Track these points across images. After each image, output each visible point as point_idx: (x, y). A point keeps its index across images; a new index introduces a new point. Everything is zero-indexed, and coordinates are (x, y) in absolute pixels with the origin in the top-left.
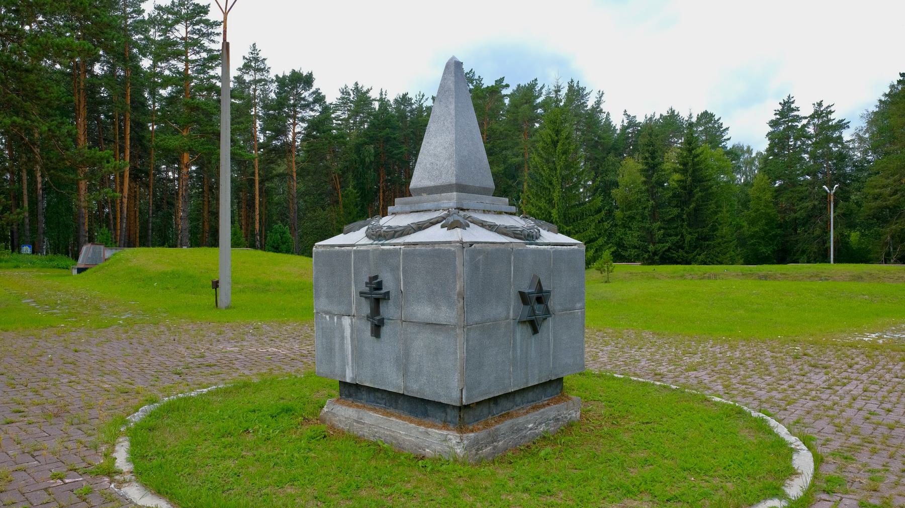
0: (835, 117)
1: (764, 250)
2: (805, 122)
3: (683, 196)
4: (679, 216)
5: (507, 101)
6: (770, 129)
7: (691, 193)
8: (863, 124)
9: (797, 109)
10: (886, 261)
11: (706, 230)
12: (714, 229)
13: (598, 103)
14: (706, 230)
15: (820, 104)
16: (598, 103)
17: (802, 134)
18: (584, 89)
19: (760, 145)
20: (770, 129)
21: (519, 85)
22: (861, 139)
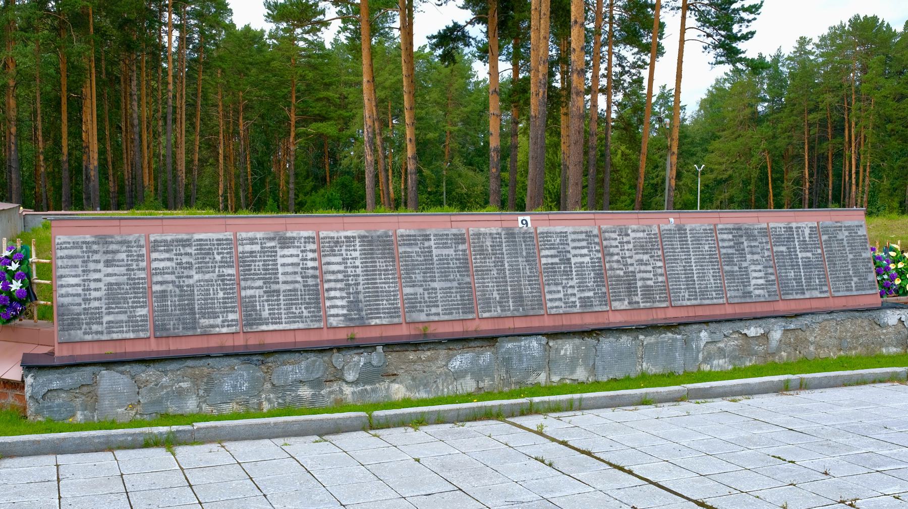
15: (664, 87)
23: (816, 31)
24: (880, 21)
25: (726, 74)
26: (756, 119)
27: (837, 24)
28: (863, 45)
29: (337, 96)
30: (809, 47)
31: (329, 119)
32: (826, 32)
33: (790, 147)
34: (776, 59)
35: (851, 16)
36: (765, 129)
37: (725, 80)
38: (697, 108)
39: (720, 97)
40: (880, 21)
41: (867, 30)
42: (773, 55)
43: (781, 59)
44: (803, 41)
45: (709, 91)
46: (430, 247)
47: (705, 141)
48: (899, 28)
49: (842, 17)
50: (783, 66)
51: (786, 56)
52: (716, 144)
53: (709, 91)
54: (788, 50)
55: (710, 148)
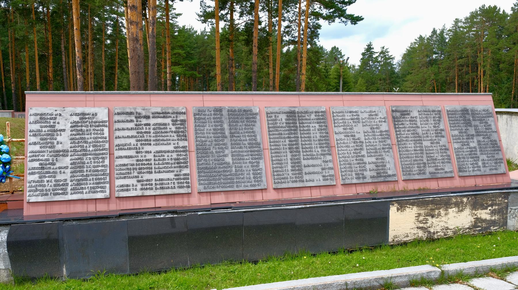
2: (377, 55)
15: (383, 48)
23: (464, 14)
24: (498, 8)
25: (416, 40)
26: (432, 63)
27: (474, 10)
28: (489, 22)
29: (184, 52)
30: (460, 24)
31: (179, 64)
32: (468, 15)
33: (448, 78)
34: (442, 32)
35: (480, 5)
36: (434, 68)
37: (415, 43)
38: (401, 59)
39: (413, 52)
40: (498, 8)
41: (489, 14)
42: (441, 29)
43: (445, 31)
44: (457, 21)
45: (407, 49)
46: (469, 120)
47: (404, 75)
48: (509, 12)
49: (475, 7)
50: (447, 34)
51: (448, 29)
52: (409, 77)
53: (407, 49)
54: (449, 25)
55: (406, 79)
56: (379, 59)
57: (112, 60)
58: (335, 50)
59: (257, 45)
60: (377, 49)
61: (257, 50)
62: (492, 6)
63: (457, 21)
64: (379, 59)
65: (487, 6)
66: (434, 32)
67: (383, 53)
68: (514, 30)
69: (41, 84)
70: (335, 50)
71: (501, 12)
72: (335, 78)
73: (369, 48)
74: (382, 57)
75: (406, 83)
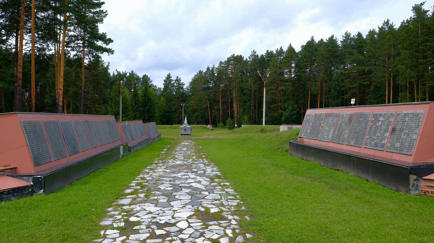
0: (182, 81)
1: (164, 120)
2: (174, 82)
3: (145, 104)
4: (144, 111)
5: (142, 80)
6: (164, 83)
7: (147, 104)
8: (188, 85)
9: (171, 77)
10: (194, 124)
11: (151, 115)
12: (153, 114)
13: (108, 66)
14: (151, 115)
15: (178, 77)
16: (108, 66)
17: (173, 85)
18: (103, 61)
19: (162, 87)
20: (164, 83)
21: (267, 51)
22: (188, 89)
56: (175, 84)
57: (364, 92)
58: (145, 77)
59: (21, 65)
60: (174, 78)
61: (22, 69)
62: (239, 55)
63: (221, 63)
64: (175, 84)
65: (236, 55)
66: (208, 68)
67: (178, 80)
68: (250, 70)
69: (392, 101)
70: (145, 77)
71: (245, 59)
72: (142, 96)
73: (169, 77)
74: (177, 83)
75: (191, 101)
